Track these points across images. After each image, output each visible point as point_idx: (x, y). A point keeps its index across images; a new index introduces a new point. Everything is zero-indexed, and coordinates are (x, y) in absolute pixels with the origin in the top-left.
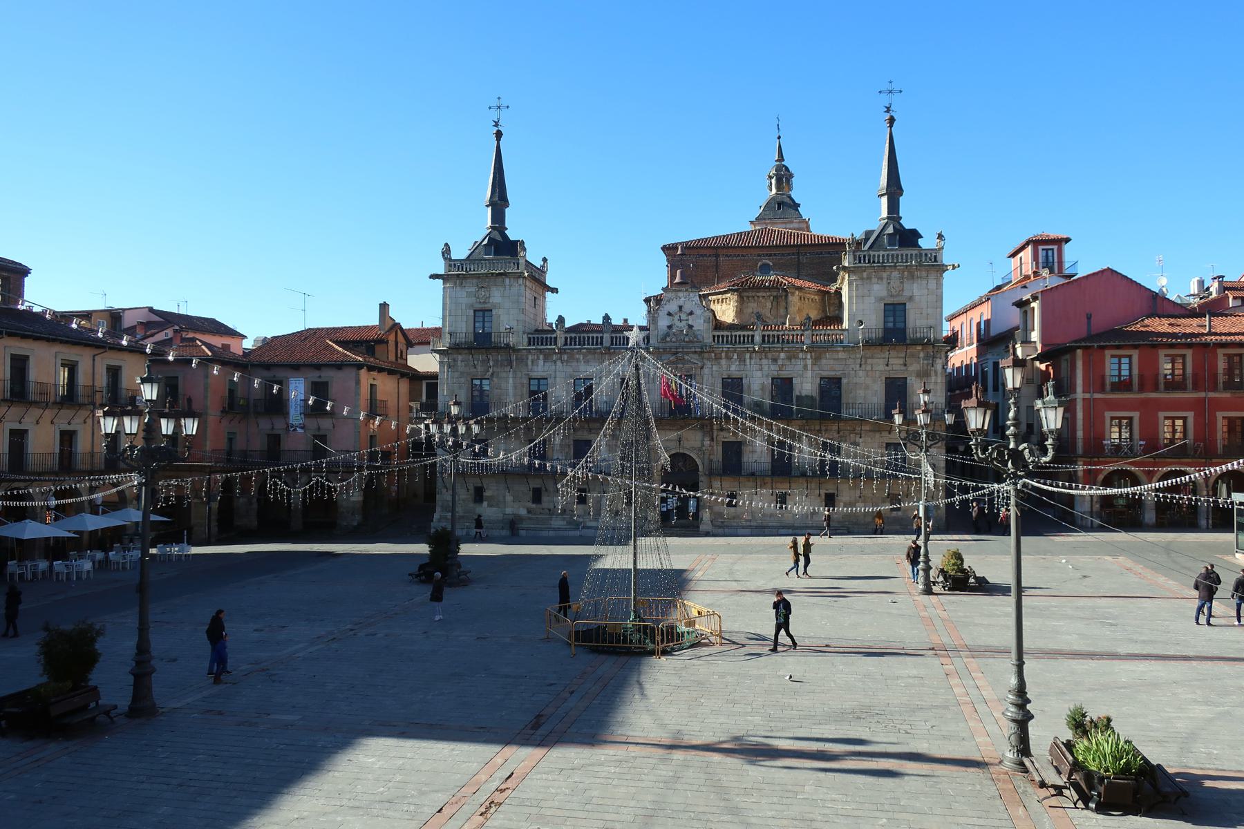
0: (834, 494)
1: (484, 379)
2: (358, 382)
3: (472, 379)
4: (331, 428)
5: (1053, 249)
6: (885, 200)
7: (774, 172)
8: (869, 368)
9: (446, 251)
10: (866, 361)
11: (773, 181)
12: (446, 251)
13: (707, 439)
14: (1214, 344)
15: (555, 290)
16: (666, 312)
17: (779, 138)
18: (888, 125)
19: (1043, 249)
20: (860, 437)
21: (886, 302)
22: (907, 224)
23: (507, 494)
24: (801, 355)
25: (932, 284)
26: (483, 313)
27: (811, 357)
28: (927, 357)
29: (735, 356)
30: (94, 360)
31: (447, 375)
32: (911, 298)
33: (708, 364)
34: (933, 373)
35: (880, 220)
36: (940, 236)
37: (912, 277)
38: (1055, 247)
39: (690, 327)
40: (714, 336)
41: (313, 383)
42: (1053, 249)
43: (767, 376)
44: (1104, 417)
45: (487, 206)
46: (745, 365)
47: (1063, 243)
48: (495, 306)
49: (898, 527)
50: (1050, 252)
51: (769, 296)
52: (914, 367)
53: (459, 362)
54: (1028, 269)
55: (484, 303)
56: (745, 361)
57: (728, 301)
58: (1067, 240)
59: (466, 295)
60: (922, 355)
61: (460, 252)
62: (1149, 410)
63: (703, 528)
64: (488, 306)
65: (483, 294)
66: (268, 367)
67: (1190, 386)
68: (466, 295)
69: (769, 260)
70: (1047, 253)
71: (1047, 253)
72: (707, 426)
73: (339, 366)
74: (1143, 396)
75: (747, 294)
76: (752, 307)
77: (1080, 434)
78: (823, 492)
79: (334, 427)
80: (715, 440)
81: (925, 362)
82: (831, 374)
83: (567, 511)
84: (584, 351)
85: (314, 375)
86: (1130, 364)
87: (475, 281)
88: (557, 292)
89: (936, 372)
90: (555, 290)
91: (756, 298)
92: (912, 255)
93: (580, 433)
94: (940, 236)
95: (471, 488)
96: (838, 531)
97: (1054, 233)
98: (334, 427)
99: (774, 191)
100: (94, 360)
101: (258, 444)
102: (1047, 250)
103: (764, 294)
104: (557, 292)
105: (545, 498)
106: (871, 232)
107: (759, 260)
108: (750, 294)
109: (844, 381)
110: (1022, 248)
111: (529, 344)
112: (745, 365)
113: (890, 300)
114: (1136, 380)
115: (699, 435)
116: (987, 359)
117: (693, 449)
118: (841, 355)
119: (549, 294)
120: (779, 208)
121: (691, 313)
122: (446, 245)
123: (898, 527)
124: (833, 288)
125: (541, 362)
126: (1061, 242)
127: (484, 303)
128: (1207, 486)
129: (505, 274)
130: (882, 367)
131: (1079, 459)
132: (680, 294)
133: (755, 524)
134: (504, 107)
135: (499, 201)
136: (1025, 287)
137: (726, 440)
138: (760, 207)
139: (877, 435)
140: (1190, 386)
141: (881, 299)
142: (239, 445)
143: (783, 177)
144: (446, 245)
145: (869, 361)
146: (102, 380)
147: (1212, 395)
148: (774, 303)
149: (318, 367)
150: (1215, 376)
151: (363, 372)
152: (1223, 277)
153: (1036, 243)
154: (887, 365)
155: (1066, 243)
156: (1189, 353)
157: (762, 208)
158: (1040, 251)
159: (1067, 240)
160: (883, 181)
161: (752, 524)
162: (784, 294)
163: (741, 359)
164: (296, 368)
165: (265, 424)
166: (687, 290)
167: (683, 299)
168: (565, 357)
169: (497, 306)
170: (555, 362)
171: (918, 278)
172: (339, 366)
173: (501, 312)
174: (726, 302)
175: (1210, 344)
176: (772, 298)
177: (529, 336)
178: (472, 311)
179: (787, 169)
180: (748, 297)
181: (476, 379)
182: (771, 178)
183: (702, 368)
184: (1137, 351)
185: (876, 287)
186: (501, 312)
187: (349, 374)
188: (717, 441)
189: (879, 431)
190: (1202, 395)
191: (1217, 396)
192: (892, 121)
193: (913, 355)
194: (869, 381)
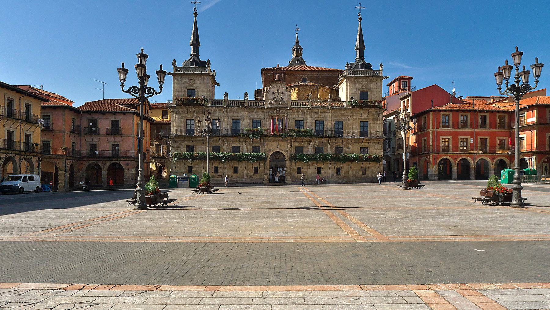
0: (340, 168)
1: (192, 119)
2: (133, 121)
3: (186, 120)
4: (121, 141)
5: (406, 82)
6: (358, 51)
7: (295, 47)
8: (354, 117)
9: (174, 63)
10: (353, 114)
11: (295, 52)
12: (174, 63)
13: (289, 145)
14: (478, 111)
15: (218, 85)
16: (272, 92)
17: (297, 33)
18: (359, 21)
19: (403, 82)
20: (351, 145)
21: (361, 91)
22: (367, 61)
23: (203, 169)
24: (327, 111)
25: (378, 83)
26: (191, 92)
27: (331, 112)
28: (376, 113)
29: (301, 111)
30: (20, 99)
31: (175, 117)
32: (370, 90)
33: (290, 114)
34: (378, 120)
35: (356, 59)
36: (381, 65)
37: (370, 81)
38: (407, 81)
39: (282, 98)
40: (292, 103)
41: (112, 120)
42: (406, 82)
43: (314, 120)
44: (440, 138)
45: (191, 45)
46: (305, 115)
47: (410, 80)
48: (196, 88)
49: (365, 181)
50: (405, 83)
51: (311, 89)
52: (371, 117)
53: (181, 112)
54: (397, 89)
55: (192, 86)
56: (305, 113)
57: (293, 91)
58: (412, 78)
59: (184, 83)
60: (374, 113)
61: (180, 64)
62: (455, 135)
63: (287, 182)
64: (193, 88)
65: (191, 82)
66: (90, 113)
67: (469, 126)
68: (184, 83)
69: (306, 76)
70: (404, 83)
71: (404, 83)
72: (289, 140)
73: (124, 113)
74: (453, 130)
75: (301, 88)
76: (303, 93)
77: (431, 144)
78: (336, 167)
79: (122, 141)
80: (292, 146)
81: (375, 115)
82: (340, 119)
83: (229, 176)
84: (237, 107)
85: (112, 118)
86: (449, 118)
87: (188, 76)
88: (219, 85)
89: (379, 119)
90: (218, 85)
91: (305, 90)
92: (370, 72)
93: (235, 143)
94: (381, 65)
95: (187, 167)
96: (342, 183)
97: (407, 76)
98: (122, 141)
99: (295, 55)
100: (20, 99)
101: (85, 148)
102: (404, 82)
103: (308, 88)
104: (219, 85)
105: (219, 171)
106: (352, 64)
107: (302, 76)
108: (303, 88)
109: (344, 122)
110: (395, 81)
111: (212, 105)
112: (305, 115)
113: (362, 90)
114: (451, 124)
115: (286, 144)
116: (387, 121)
117: (283, 150)
118: (343, 112)
119: (216, 86)
120: (297, 62)
121: (282, 93)
122: (174, 60)
123: (365, 181)
124: (334, 88)
125: (217, 113)
126: (409, 79)
127: (192, 86)
128: (474, 164)
129: (202, 74)
130: (359, 117)
131: (431, 154)
132: (278, 85)
133: (309, 180)
134: (362, 8)
135: (196, 44)
136: (398, 95)
137: (297, 146)
138: (289, 62)
139: (357, 144)
140: (469, 126)
141: (359, 89)
142: (77, 148)
143: (298, 50)
144: (174, 60)
145: (354, 114)
146: (24, 109)
147: (476, 130)
148: (313, 92)
149: (114, 113)
150: (477, 123)
151: (135, 116)
152: (462, 97)
153: (400, 79)
154: (361, 116)
155: (411, 79)
156: (469, 114)
157: (290, 62)
158: (402, 82)
159: (412, 78)
160: (358, 43)
161: (307, 180)
162: (317, 88)
163: (303, 113)
164: (104, 113)
165: (89, 139)
166: (280, 83)
167: (279, 87)
168: (228, 110)
169: (198, 88)
170: (224, 112)
171: (373, 82)
172: (124, 113)
173: (199, 90)
174: (292, 91)
175: (477, 111)
176: (311, 90)
177: (212, 101)
178: (186, 90)
179: (300, 46)
180: (302, 89)
181: (188, 119)
182: (294, 50)
183: (287, 116)
184: (451, 113)
185: (357, 85)
186: (199, 90)
187: (129, 116)
188: (293, 146)
189: (358, 143)
190: (473, 130)
191: (478, 131)
192: (361, 19)
193: (371, 112)
194: (354, 122)
